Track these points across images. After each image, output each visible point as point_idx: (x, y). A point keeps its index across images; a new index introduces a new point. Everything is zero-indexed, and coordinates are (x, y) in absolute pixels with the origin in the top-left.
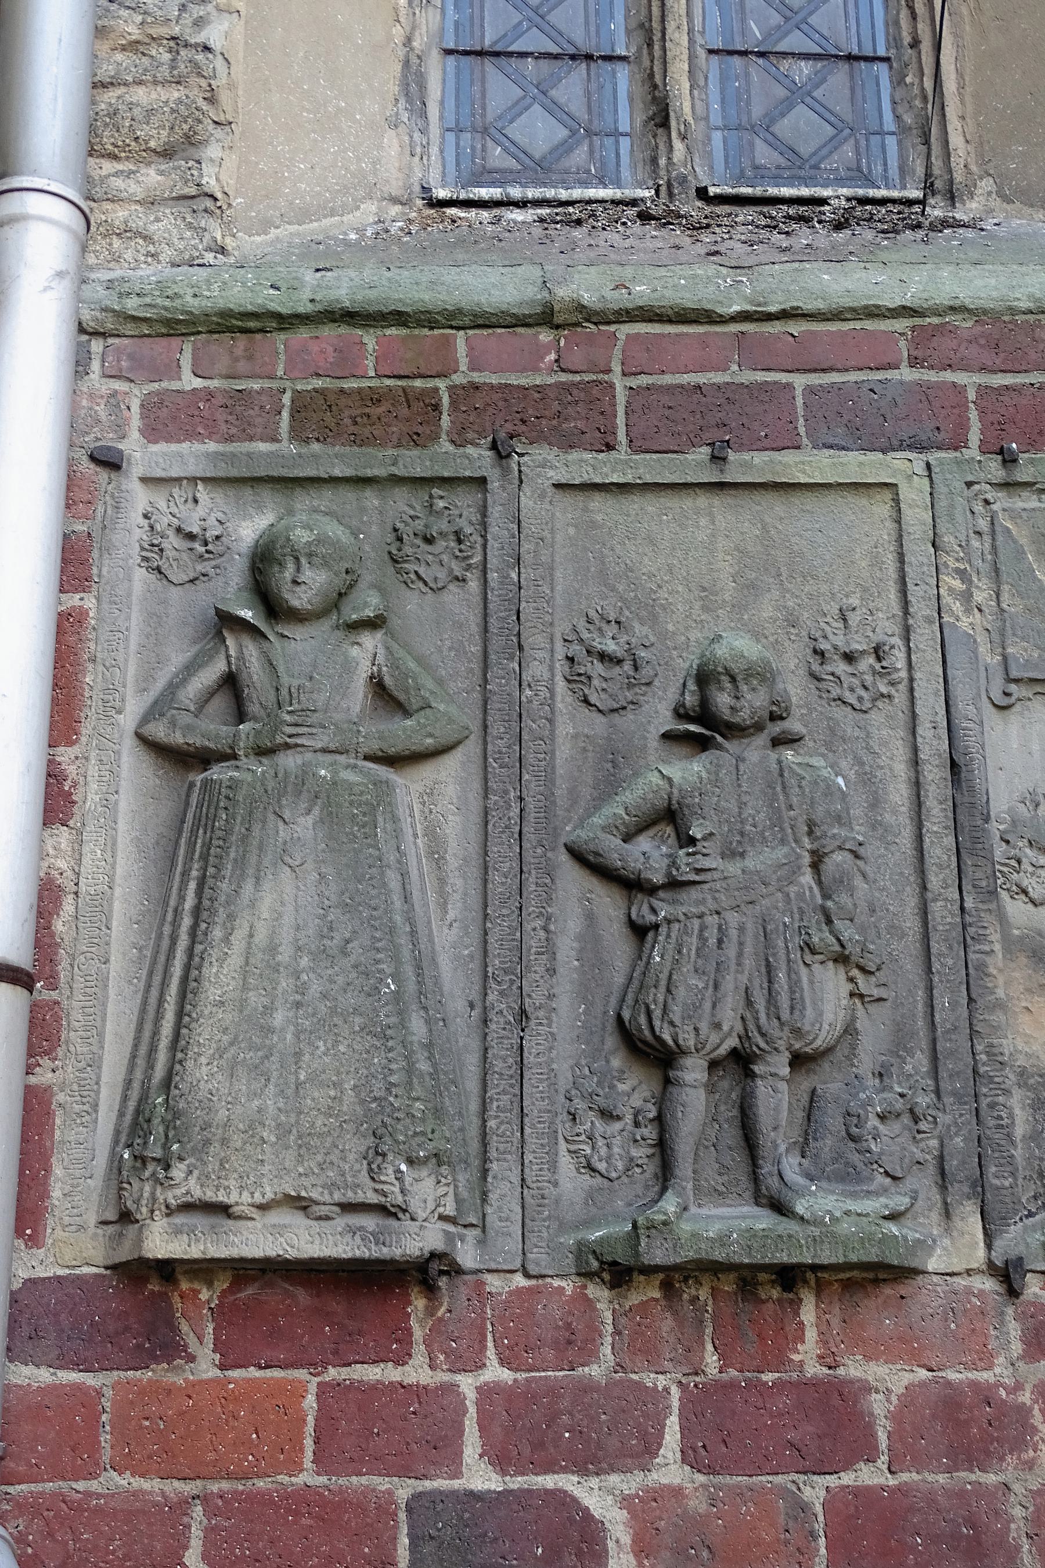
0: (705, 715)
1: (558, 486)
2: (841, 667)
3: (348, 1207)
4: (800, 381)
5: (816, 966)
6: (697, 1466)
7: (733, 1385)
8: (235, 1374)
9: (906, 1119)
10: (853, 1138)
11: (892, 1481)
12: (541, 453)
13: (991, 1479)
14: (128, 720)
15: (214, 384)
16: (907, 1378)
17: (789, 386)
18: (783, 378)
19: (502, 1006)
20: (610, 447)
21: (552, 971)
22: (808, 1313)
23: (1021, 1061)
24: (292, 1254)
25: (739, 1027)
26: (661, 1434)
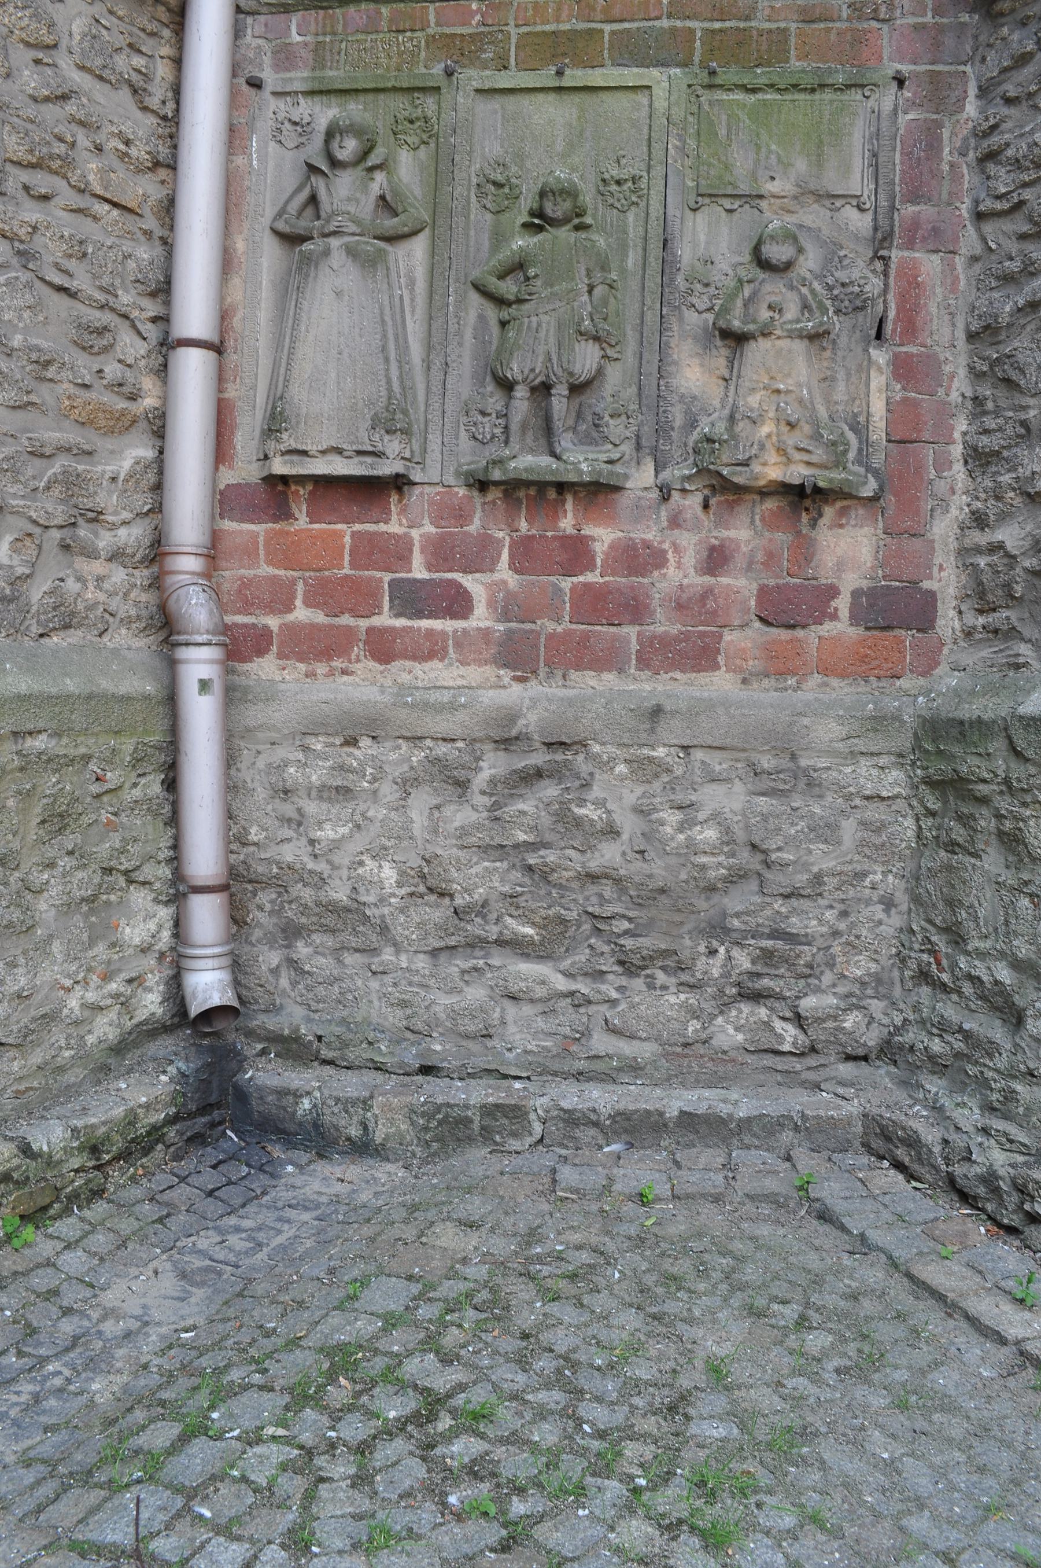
0: (539, 213)
1: (477, 91)
2: (614, 188)
3: (359, 453)
4: (608, 28)
5: (583, 343)
6: (517, 571)
7: (533, 536)
8: (316, 526)
9: (624, 417)
10: (596, 426)
11: (601, 580)
12: (472, 72)
13: (645, 581)
14: (266, 221)
15: (308, 38)
16: (613, 536)
17: (602, 31)
18: (598, 26)
19: (437, 363)
20: (505, 68)
21: (460, 344)
22: (569, 505)
23: (683, 390)
24: (335, 473)
25: (544, 370)
26: (499, 556)
